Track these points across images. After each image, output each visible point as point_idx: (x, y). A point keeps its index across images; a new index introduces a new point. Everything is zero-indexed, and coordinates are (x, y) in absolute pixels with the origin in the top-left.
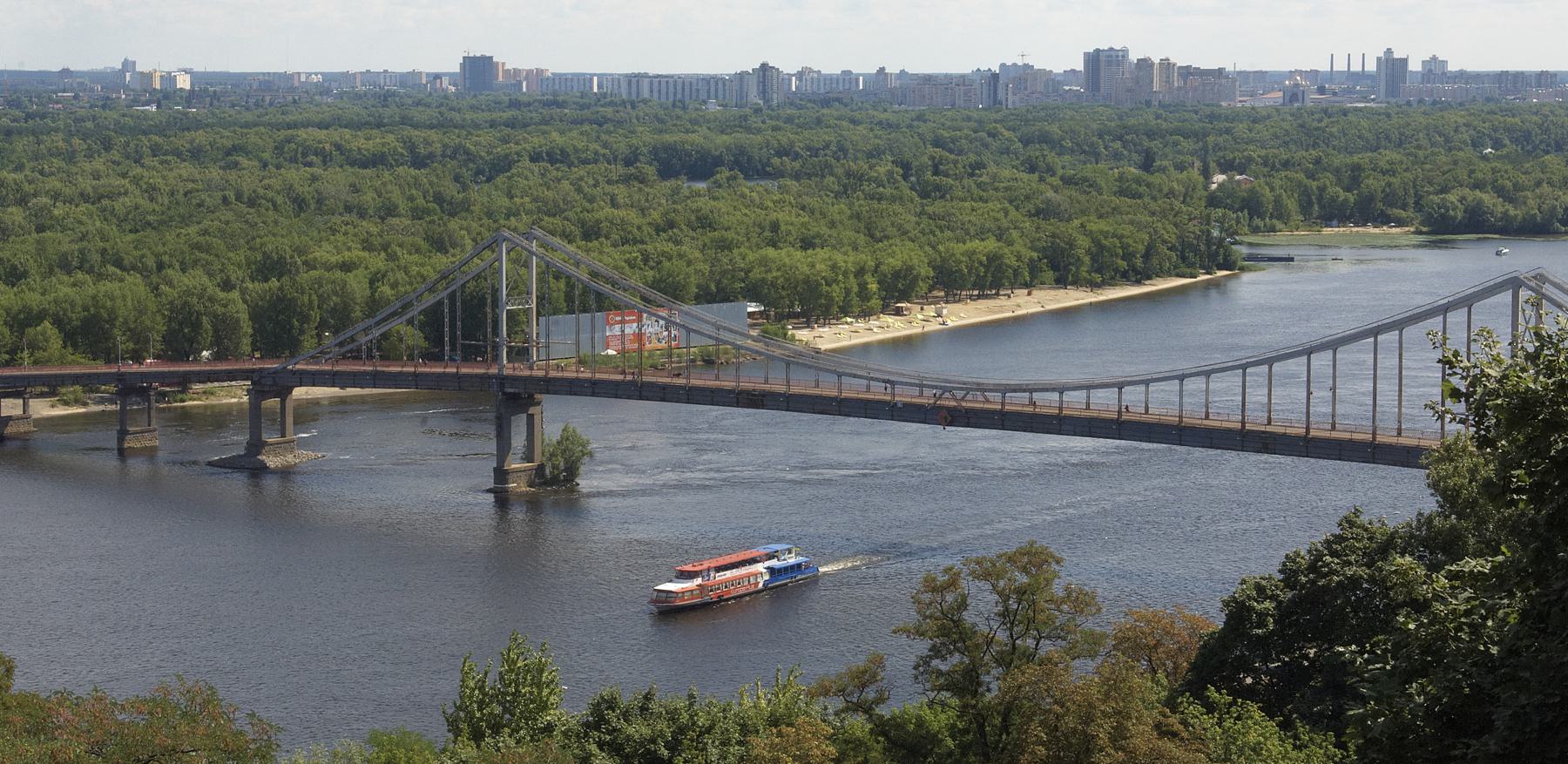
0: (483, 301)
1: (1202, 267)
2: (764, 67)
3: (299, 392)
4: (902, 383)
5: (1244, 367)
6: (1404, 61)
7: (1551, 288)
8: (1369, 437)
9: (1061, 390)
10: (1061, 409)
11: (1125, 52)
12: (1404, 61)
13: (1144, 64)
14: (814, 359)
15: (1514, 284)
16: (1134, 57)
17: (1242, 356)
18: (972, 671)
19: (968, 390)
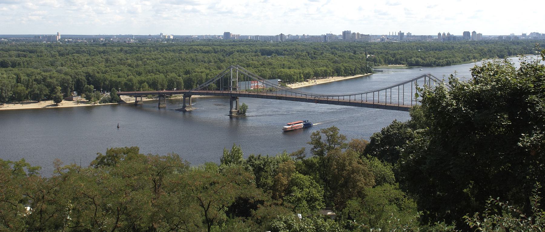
2: (281, 34)
3: (193, 96)
6: (403, 33)
11: (350, 31)
12: (403, 33)
13: (354, 34)
15: (425, 76)
16: (352, 32)
17: (386, 87)
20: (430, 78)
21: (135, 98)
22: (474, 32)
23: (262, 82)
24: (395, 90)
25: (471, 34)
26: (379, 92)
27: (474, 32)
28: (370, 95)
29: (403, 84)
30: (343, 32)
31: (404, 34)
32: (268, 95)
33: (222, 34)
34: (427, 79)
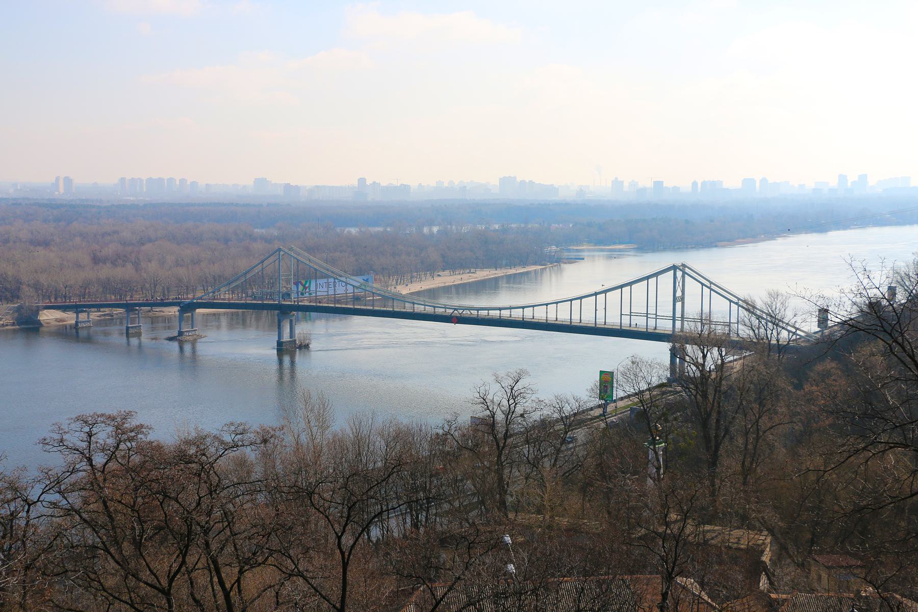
0: (531, 280)
1: (549, 262)
2: (374, 182)
3: (198, 311)
4: (437, 307)
5: (571, 300)
6: (622, 182)
7: (688, 270)
8: (569, 323)
9: (500, 309)
10: (647, 329)
11: (515, 178)
12: (622, 182)
13: (523, 182)
14: (402, 299)
15: (674, 268)
16: (519, 180)
17: (570, 296)
18: (70, 301)
19: (464, 310)
20: (684, 273)
21: (75, 315)
22: (764, 180)
23: (344, 282)
24: (614, 296)
25: (758, 185)
26: (657, 278)
27: (764, 180)
28: (564, 308)
29: (656, 275)
30: (500, 178)
31: (663, 185)
32: (356, 307)
33: (649, 184)
34: (679, 274)
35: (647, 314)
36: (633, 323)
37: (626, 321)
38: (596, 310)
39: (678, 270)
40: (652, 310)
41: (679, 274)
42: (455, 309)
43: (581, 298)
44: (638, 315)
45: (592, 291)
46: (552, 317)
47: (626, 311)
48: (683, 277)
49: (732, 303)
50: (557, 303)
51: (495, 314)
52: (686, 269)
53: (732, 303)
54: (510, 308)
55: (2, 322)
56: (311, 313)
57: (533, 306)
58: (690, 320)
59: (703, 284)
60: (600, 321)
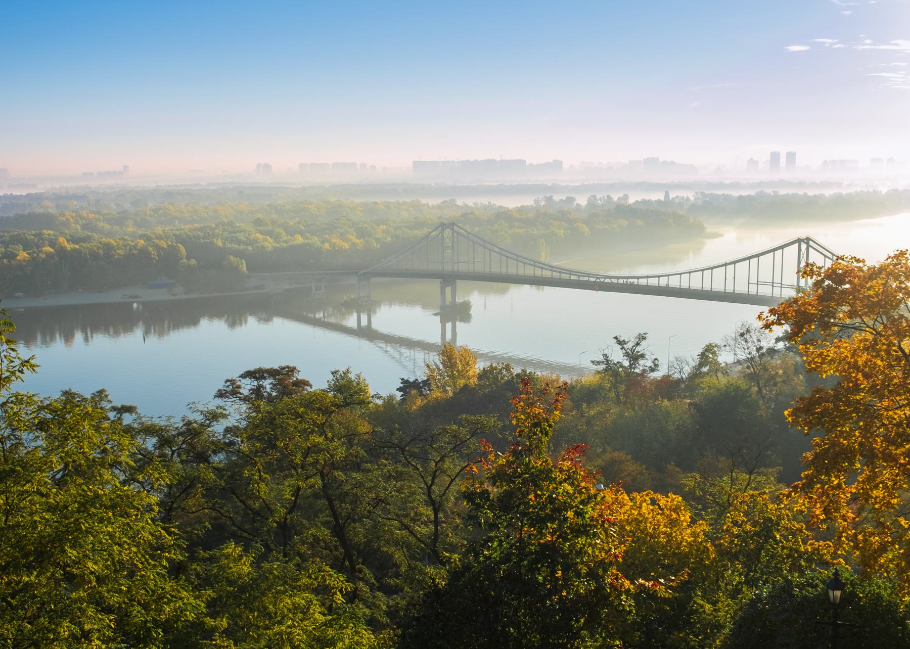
5: (703, 270)
15: (799, 241)
20: (808, 246)
24: (742, 266)
29: (782, 247)
34: (804, 246)
35: (773, 283)
36: (543, 274)
37: (753, 290)
38: (726, 279)
39: (797, 244)
40: (777, 279)
41: (804, 246)
42: (598, 278)
43: (712, 268)
44: (765, 283)
45: (723, 262)
46: (685, 285)
47: (753, 280)
48: (807, 249)
49: (492, 252)
50: (690, 273)
51: (653, 282)
52: (810, 242)
53: (492, 252)
54: (648, 277)
55: (909, 494)
56: (545, 287)
57: (668, 276)
58: (539, 265)
59: (825, 256)
60: (730, 289)
